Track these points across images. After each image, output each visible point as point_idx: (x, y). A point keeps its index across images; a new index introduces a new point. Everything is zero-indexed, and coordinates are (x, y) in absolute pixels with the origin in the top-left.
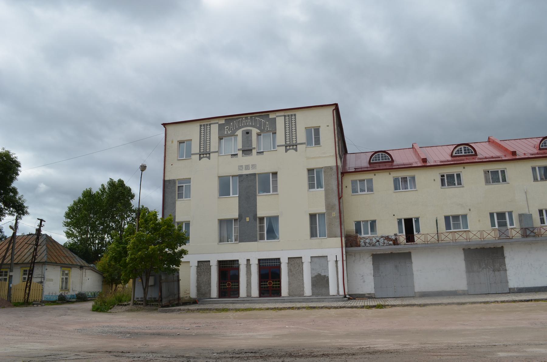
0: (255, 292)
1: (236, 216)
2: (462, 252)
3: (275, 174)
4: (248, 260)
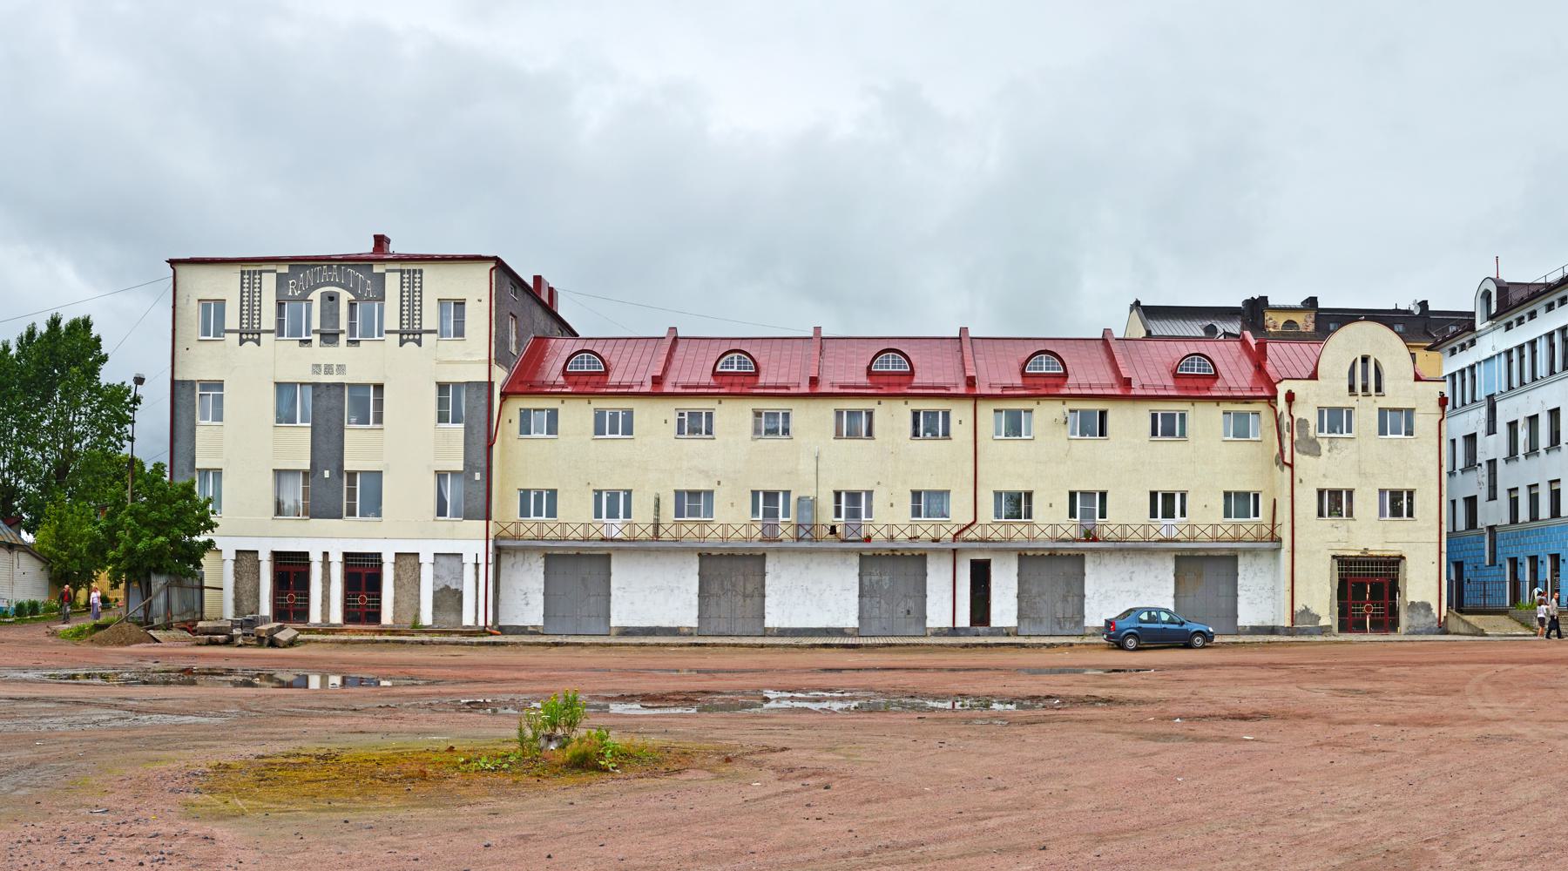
0: (336, 616)
1: (459, 465)
2: (694, 566)
3: (379, 388)
4: (326, 554)
